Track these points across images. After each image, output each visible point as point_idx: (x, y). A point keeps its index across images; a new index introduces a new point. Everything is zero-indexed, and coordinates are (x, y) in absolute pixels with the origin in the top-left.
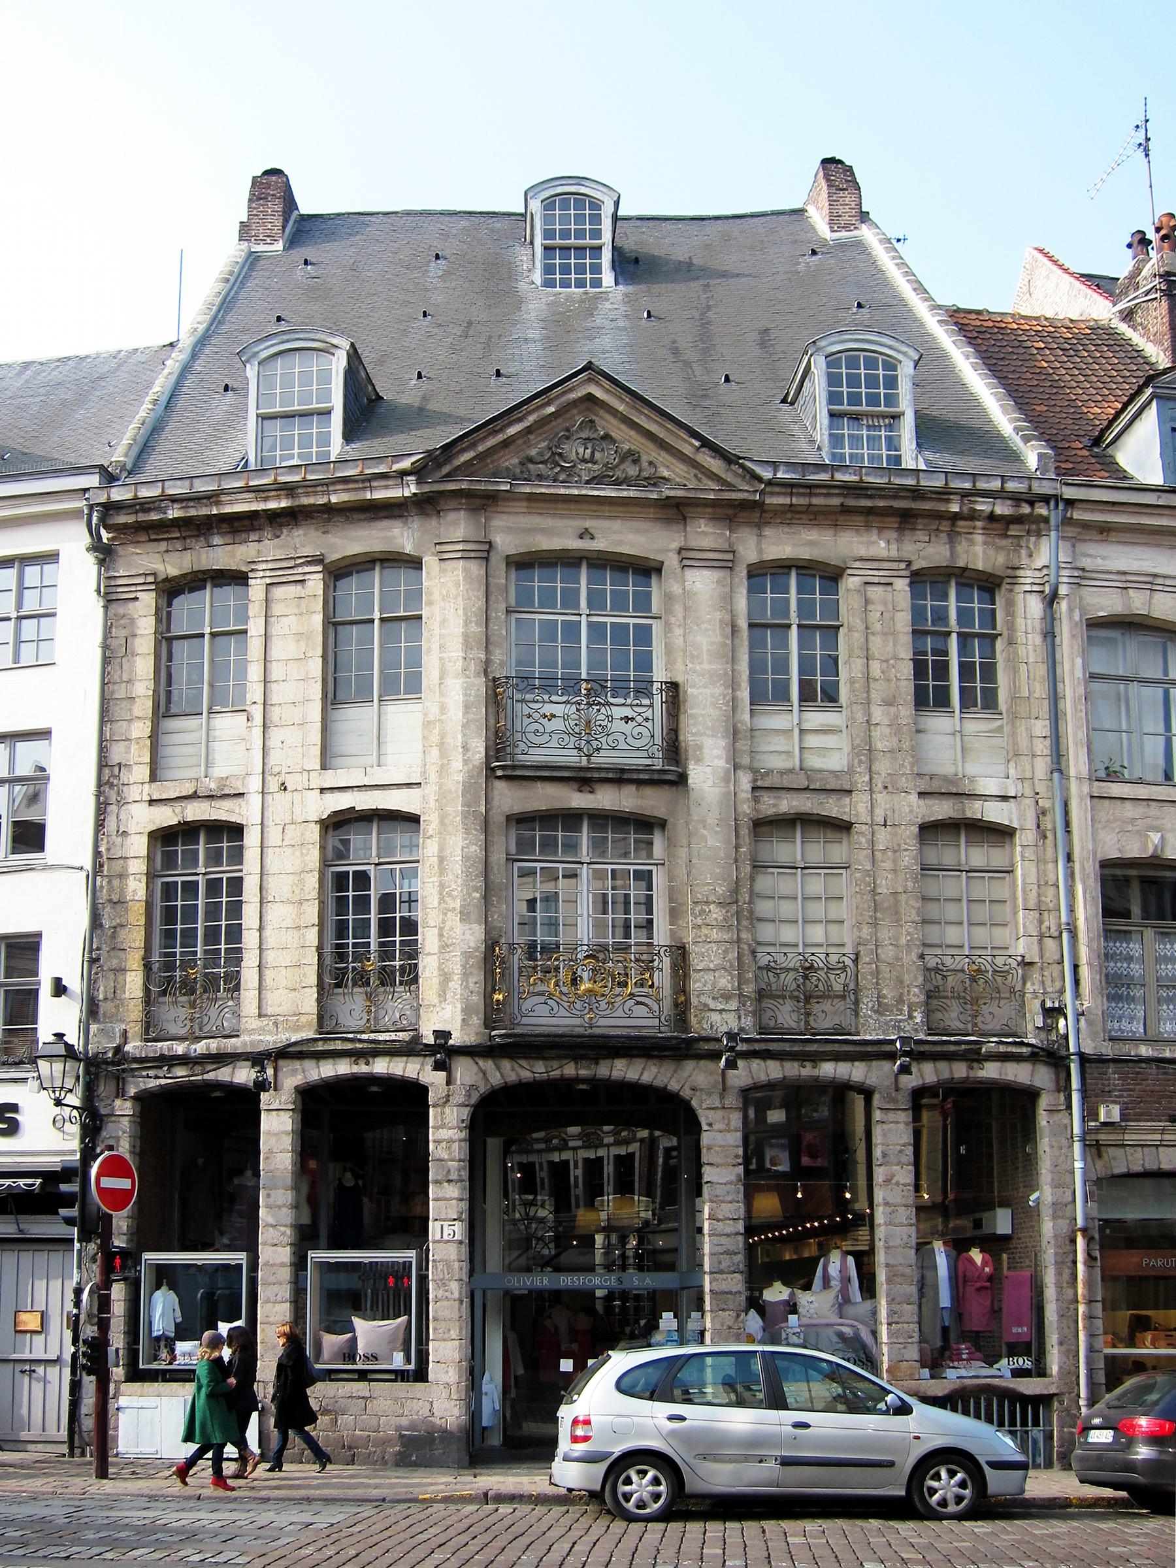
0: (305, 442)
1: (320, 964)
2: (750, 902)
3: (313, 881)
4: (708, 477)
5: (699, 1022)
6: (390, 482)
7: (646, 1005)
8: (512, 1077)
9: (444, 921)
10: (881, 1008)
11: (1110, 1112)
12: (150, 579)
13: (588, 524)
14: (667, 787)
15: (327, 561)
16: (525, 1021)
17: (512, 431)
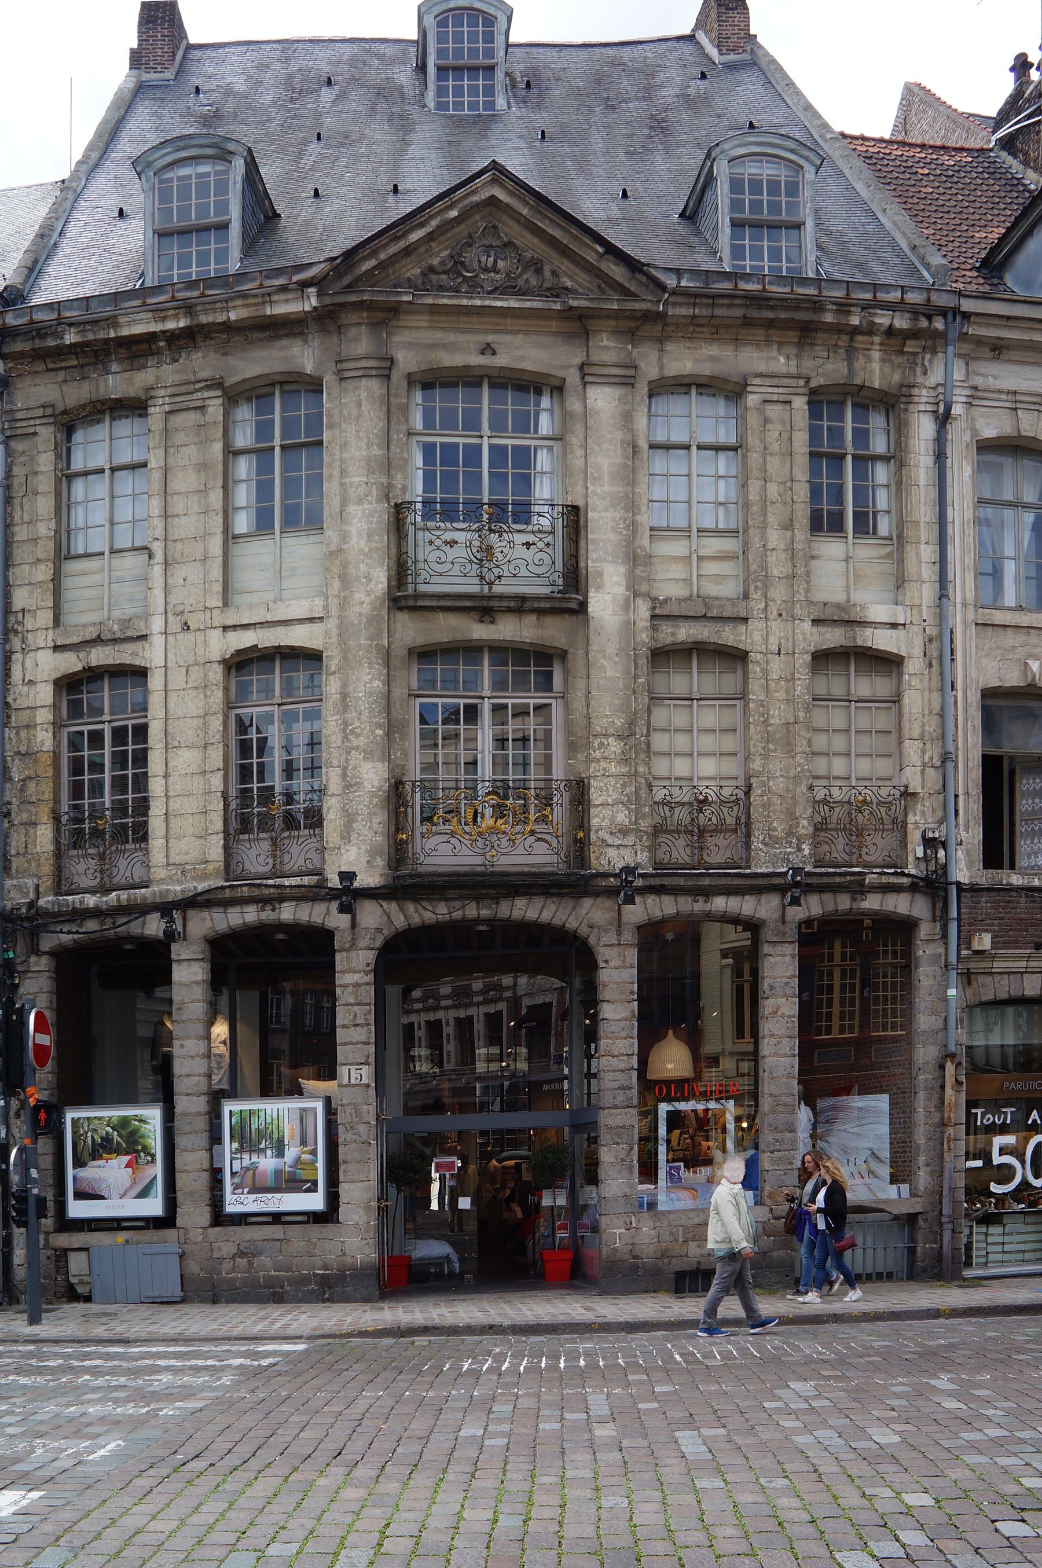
0: (203, 259)
1: (226, 806)
2: (648, 735)
3: (216, 723)
4: (611, 287)
5: (597, 859)
6: (290, 296)
7: (546, 841)
8: (416, 920)
9: (347, 761)
10: (771, 841)
11: (984, 941)
12: (49, 411)
13: (490, 338)
14: (567, 616)
15: (227, 384)
16: (428, 861)
17: (415, 236)
